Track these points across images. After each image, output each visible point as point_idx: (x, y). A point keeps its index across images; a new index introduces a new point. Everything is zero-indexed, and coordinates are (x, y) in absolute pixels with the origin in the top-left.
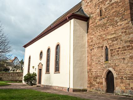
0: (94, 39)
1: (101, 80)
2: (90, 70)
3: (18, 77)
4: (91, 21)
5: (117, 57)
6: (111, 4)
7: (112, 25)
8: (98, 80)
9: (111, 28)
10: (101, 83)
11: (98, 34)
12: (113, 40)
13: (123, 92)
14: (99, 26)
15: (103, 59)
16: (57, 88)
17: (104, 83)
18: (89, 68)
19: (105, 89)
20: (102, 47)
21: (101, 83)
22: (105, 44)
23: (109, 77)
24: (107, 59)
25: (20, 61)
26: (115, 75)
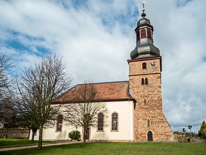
0: (140, 114)
1: (145, 136)
2: (137, 130)
3: (21, 135)
4: (137, 104)
5: (155, 125)
6: (50, 90)
7: (153, 110)
8: (143, 136)
10: (145, 137)
12: (153, 117)
14: (144, 108)
15: (146, 125)
16: (115, 141)
17: (147, 137)
18: (136, 129)
19: (147, 140)
21: (145, 137)
22: (148, 118)
23: (150, 135)
24: (149, 126)
25: (45, 138)
26: (153, 133)
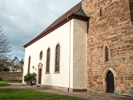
0: (94, 39)
1: (101, 80)
2: (90, 70)
3: (18, 77)
4: (91, 21)
5: (117, 57)
6: (111, 4)
7: (112, 25)
8: (98, 80)
10: (101, 83)
12: (113, 40)
14: (99, 26)
15: (103, 59)
16: (57, 88)
17: (104, 83)
18: (89, 68)
19: (105, 89)
21: (101, 83)
22: (105, 44)
23: (109, 77)
24: (107, 59)
25: (20, 61)
26: (115, 75)
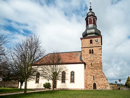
2: (86, 82)
3: (13, 85)
5: (98, 79)
6: (32, 57)
7: (96, 70)
8: (90, 86)
9: (96, 70)
10: (92, 87)
11: (90, 71)
13: (85, 89)
15: (92, 79)
16: (73, 89)
17: (93, 87)
19: (93, 88)
20: (92, 75)
21: (92, 87)
22: (93, 75)
23: (95, 85)
24: (94, 79)
26: (97, 84)
